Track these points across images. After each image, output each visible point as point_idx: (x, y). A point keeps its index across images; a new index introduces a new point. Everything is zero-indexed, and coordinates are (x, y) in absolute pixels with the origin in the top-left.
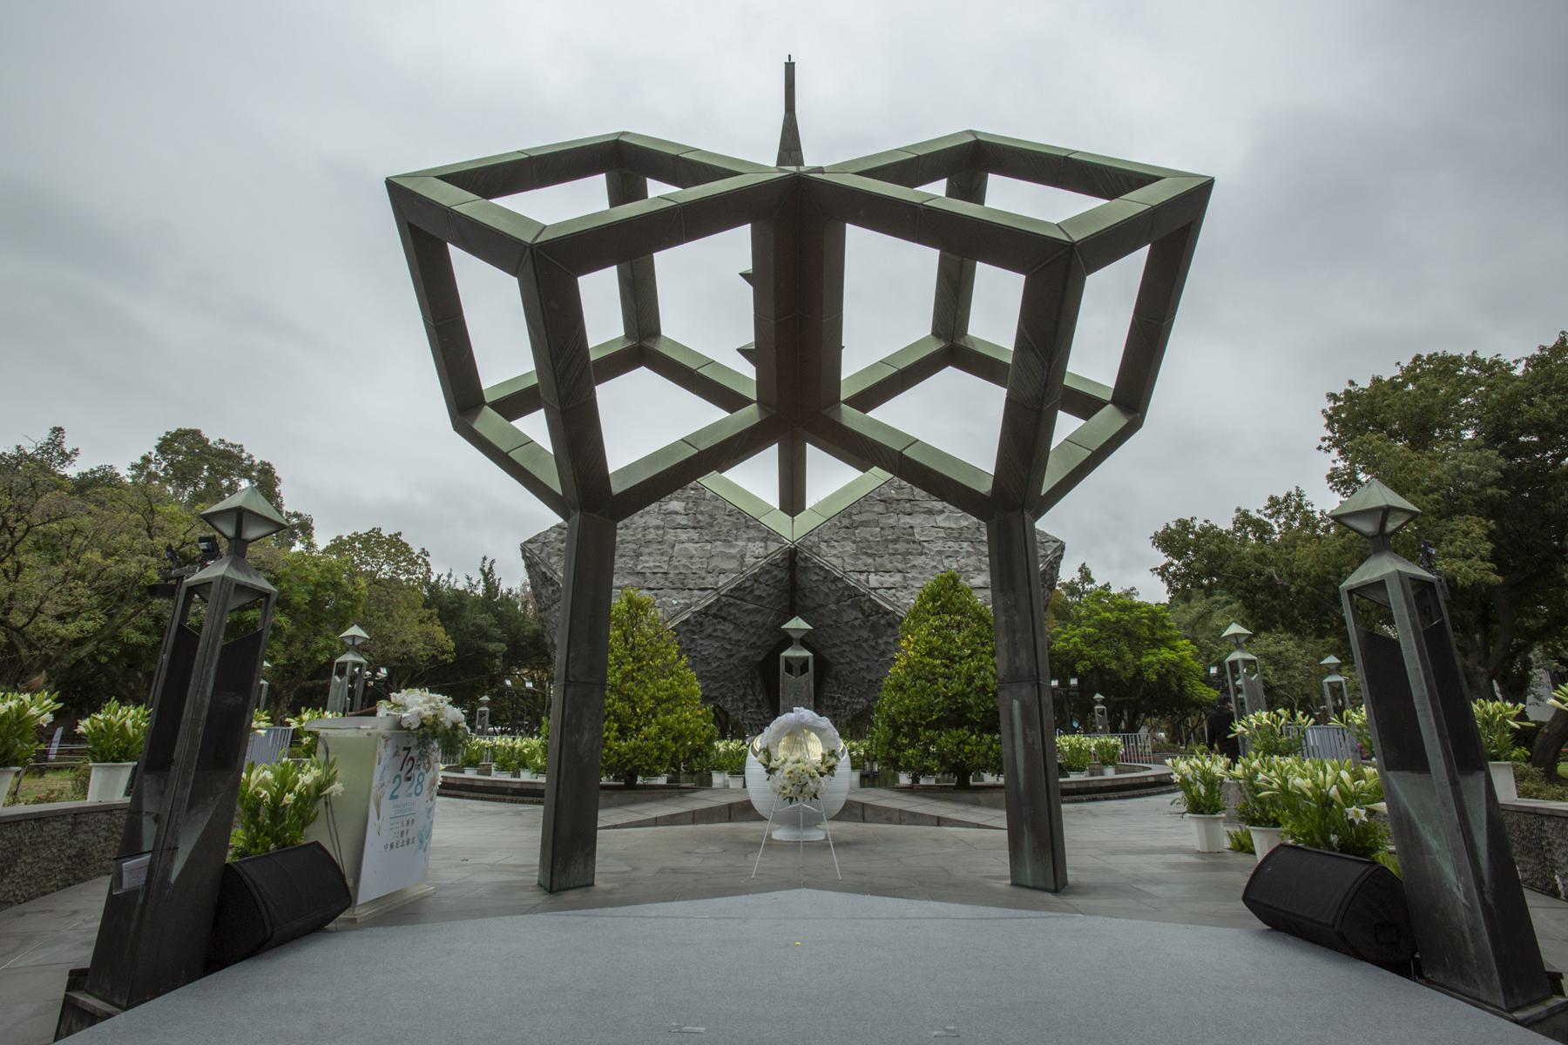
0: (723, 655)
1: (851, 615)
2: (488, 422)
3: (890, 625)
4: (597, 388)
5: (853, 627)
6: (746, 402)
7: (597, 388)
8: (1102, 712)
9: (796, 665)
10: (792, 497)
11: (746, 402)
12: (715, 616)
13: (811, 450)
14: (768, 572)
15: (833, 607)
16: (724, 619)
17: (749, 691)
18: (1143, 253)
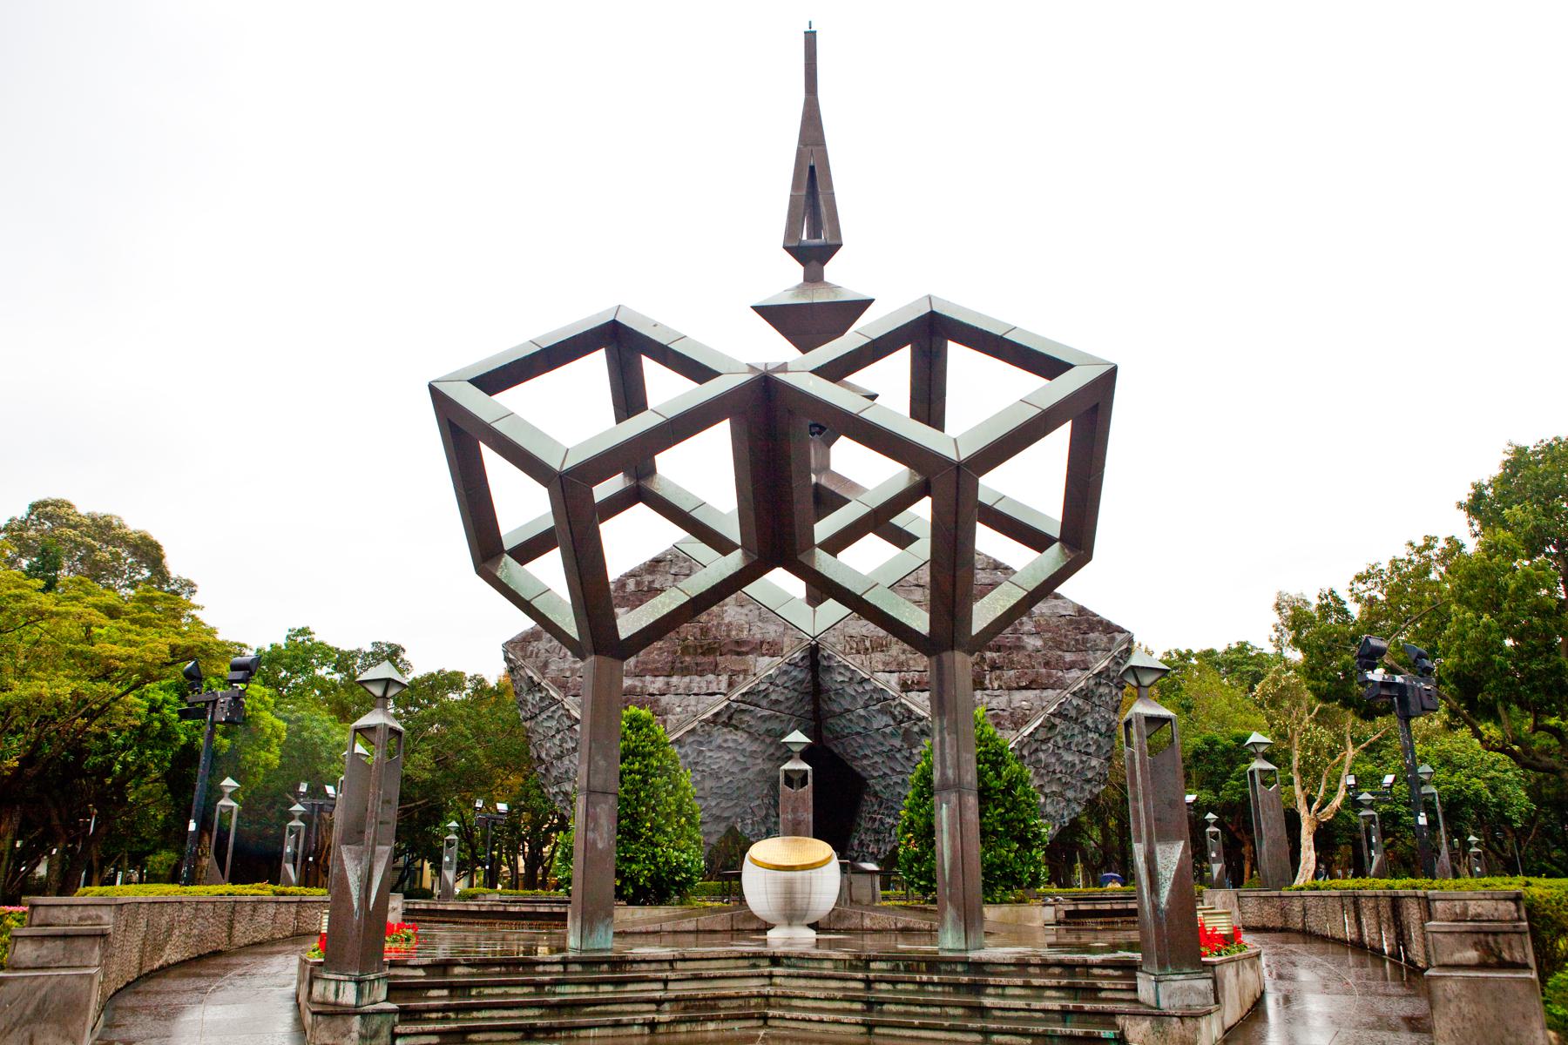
0: (735, 769)
1: (880, 721)
2: (509, 568)
4: (602, 527)
5: (884, 735)
6: (734, 547)
7: (602, 527)
8: (1215, 836)
9: (796, 777)
11: (734, 547)
12: (725, 725)
14: (786, 672)
15: (862, 712)
16: (736, 728)
17: (772, 812)
18: (1067, 426)
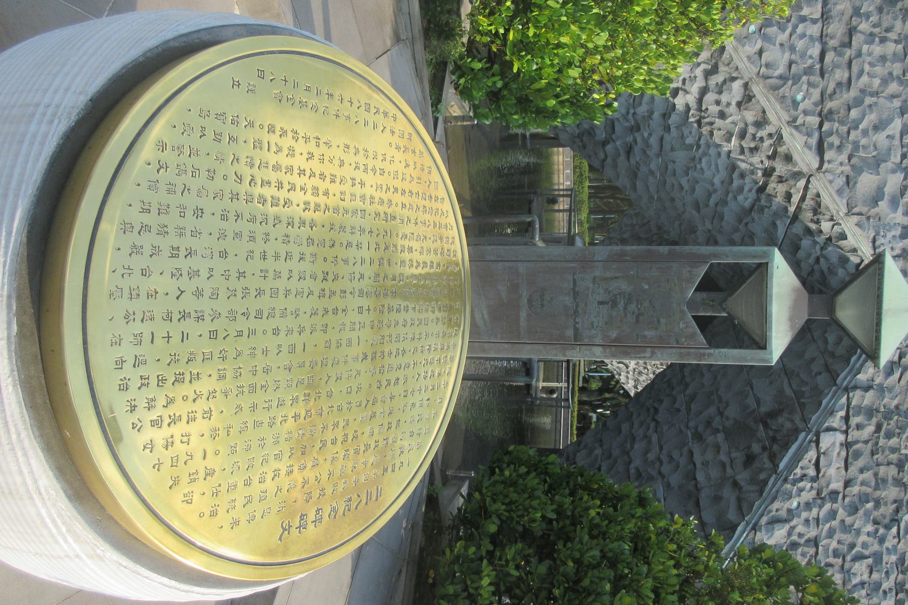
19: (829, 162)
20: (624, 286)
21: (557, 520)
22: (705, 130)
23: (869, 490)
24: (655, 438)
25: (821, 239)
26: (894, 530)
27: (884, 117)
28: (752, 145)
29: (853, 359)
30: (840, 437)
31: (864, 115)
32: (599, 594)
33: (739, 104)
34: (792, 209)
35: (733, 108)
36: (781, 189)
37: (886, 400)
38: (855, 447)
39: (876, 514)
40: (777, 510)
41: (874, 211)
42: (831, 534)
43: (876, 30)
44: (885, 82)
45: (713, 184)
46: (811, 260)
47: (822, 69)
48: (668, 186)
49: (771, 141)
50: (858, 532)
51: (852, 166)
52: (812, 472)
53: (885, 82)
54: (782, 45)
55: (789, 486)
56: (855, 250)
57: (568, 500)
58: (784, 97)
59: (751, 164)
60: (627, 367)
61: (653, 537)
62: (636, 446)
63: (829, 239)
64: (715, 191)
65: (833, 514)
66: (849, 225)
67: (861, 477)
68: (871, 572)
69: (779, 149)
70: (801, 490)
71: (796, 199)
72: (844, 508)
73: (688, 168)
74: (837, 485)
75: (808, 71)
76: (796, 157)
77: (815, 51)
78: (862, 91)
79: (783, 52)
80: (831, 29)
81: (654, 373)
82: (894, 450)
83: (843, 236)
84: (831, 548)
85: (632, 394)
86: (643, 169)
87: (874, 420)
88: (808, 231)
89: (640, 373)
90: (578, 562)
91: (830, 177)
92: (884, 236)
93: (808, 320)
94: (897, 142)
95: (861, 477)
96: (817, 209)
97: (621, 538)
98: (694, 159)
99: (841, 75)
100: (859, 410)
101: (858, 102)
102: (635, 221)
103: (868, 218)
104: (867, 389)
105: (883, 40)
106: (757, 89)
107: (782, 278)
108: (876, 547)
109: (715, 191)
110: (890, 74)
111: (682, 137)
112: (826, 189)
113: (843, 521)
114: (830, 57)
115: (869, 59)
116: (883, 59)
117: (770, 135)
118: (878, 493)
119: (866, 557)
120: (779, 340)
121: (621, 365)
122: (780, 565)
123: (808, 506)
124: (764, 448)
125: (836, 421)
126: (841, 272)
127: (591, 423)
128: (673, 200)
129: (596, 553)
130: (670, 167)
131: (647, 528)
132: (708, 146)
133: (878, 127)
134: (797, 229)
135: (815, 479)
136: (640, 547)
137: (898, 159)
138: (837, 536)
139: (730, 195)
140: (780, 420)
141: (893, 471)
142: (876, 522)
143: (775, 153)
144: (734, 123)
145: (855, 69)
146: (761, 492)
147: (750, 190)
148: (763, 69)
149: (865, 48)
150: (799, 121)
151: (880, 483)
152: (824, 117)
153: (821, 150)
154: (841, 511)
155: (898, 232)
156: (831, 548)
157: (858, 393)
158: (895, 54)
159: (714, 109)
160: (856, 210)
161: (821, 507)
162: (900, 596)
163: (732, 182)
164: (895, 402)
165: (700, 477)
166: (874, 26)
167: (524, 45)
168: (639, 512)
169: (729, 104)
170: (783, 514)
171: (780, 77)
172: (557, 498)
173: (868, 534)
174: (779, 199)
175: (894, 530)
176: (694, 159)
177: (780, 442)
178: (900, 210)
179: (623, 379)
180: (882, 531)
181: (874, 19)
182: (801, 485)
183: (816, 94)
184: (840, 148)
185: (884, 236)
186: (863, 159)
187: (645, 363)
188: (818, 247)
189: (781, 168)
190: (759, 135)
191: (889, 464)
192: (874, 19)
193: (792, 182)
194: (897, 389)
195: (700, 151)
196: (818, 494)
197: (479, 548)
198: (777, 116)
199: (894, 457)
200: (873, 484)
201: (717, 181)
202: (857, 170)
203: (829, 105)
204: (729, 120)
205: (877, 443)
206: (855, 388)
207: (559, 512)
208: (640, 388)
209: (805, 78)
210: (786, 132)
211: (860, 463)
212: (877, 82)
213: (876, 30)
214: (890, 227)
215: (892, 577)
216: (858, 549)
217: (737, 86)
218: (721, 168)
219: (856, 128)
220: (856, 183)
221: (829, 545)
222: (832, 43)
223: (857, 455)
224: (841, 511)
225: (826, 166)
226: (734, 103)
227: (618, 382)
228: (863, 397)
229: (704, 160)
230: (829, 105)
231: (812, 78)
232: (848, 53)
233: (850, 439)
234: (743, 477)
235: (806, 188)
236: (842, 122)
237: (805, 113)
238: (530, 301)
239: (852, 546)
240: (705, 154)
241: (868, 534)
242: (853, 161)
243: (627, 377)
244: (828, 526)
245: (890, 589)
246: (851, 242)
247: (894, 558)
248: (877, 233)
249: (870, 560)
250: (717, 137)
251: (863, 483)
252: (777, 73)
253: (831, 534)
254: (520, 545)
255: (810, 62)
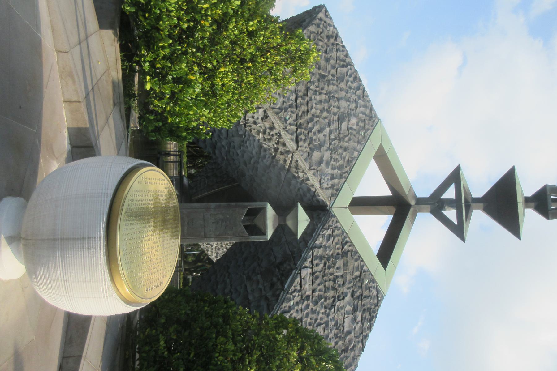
3: (272, 285)
10: (362, 204)
13: (390, 194)
19: (301, 146)
20: (221, 216)
21: (191, 313)
22: (248, 129)
23: (322, 293)
24: (228, 281)
25: (299, 180)
26: (333, 310)
27: (322, 126)
28: (269, 137)
29: (314, 234)
30: (310, 270)
31: (314, 126)
32: (210, 339)
33: (262, 119)
34: (287, 167)
35: (260, 120)
36: (282, 157)
37: (327, 252)
38: (316, 274)
39: (325, 304)
40: (284, 307)
41: (319, 168)
42: (307, 315)
43: (318, 89)
44: (322, 111)
45: (252, 154)
46: (296, 190)
47: (296, 105)
48: (231, 153)
49: (276, 137)
50: (318, 313)
51: (310, 148)
52: (298, 288)
53: (322, 111)
54: (279, 94)
55: (289, 295)
56: (313, 185)
57: (196, 304)
58: (281, 117)
59: (269, 146)
60: (212, 246)
61: (231, 315)
62: (219, 287)
63: (303, 180)
64: (253, 157)
65: (308, 306)
66: (310, 174)
67: (319, 288)
68: (324, 331)
69: (280, 140)
70: (294, 297)
71: (288, 162)
72: (312, 303)
73: (241, 146)
74: (309, 293)
75: (291, 106)
76: (287, 144)
77: (293, 97)
78: (313, 115)
79: (280, 97)
80: (299, 88)
81: (226, 248)
82: (331, 274)
83: (308, 179)
84: (308, 322)
85: (215, 261)
86: (219, 144)
87: (323, 261)
88: (294, 177)
89: (219, 249)
90: (201, 328)
91: (301, 153)
92: (324, 179)
93: (279, 225)
94: (327, 138)
95: (319, 288)
96: (297, 167)
97: (218, 317)
98: (243, 141)
99: (304, 108)
100: (317, 257)
101: (311, 120)
102: (214, 167)
103: (317, 171)
104: (320, 247)
105: (320, 93)
106: (269, 113)
107: (270, 212)
108: (326, 319)
109: (253, 157)
110: (324, 108)
111: (237, 131)
112: (299, 158)
113: (312, 309)
114: (299, 100)
115: (315, 102)
116: (320, 101)
117: (276, 134)
118: (326, 294)
119: (322, 324)
120: (270, 232)
121: (208, 246)
122: (280, 319)
123: (297, 304)
124: (278, 279)
125: (307, 263)
126: (308, 195)
127: (189, 282)
128: (234, 160)
129: (209, 323)
130: (232, 144)
131: (228, 311)
132: (249, 136)
133: (320, 131)
134: (289, 176)
135: (300, 291)
136: (226, 319)
137: (328, 145)
138: (310, 316)
139: (260, 159)
140: (285, 265)
141: (331, 283)
142: (325, 307)
143: (278, 142)
144: (261, 127)
145: (310, 105)
146: (277, 300)
147: (269, 157)
148: (272, 105)
149: (313, 96)
150: (288, 128)
151: (327, 289)
152: (299, 126)
153: (297, 142)
154: (311, 304)
155: (329, 177)
156: (308, 322)
157: (316, 249)
158: (325, 99)
159: (251, 120)
160: (312, 168)
161: (303, 303)
162: (337, 340)
163: (260, 153)
164: (331, 252)
165: (250, 297)
166: (317, 87)
167: (173, 114)
168: (225, 306)
169: (258, 119)
170: (287, 308)
171: (279, 108)
172: (191, 304)
173: (323, 313)
174: (281, 162)
175: (333, 310)
176: (243, 141)
177: (286, 275)
178: (330, 167)
179: (209, 253)
180: (328, 311)
181: (316, 84)
182: (294, 294)
183: (294, 116)
184: (305, 140)
185: (324, 179)
186: (314, 145)
187: (222, 243)
188: (298, 184)
189: (281, 149)
190: (271, 133)
191: (330, 280)
192: (316, 84)
193: (286, 155)
194: (332, 247)
195: (246, 138)
196: (302, 297)
197: (156, 330)
198: (278, 126)
199: (331, 277)
200: (324, 290)
201: (254, 152)
202: (312, 150)
203: (300, 121)
204: (258, 125)
205: (325, 272)
206: (315, 247)
207: (192, 310)
208: (219, 257)
209: (289, 109)
210: (283, 133)
211: (318, 281)
212: (318, 112)
213: (318, 89)
214: (327, 175)
215: (333, 332)
216: (319, 321)
217: (261, 111)
218: (255, 146)
219: (311, 131)
220: (312, 156)
221: (307, 321)
222: (300, 94)
223: (317, 278)
224: (311, 304)
225: (299, 148)
226: (260, 118)
227: (206, 255)
228: (318, 251)
229: (248, 142)
230: (300, 121)
231: (293, 109)
232: (307, 99)
233: (314, 271)
234: (269, 294)
235: (292, 158)
236: (305, 129)
237: (290, 124)
238: (188, 223)
239: (316, 320)
240: (248, 140)
241: (323, 313)
242: (311, 146)
243: (212, 252)
244: (306, 312)
245: (333, 337)
246: (311, 182)
247: (333, 323)
248: (321, 178)
249: (324, 325)
250: (253, 133)
251: (320, 291)
252: (278, 107)
253: (307, 315)
254: (176, 326)
255: (291, 102)
